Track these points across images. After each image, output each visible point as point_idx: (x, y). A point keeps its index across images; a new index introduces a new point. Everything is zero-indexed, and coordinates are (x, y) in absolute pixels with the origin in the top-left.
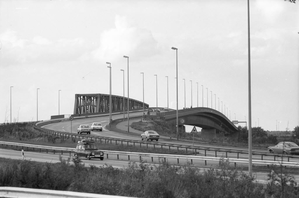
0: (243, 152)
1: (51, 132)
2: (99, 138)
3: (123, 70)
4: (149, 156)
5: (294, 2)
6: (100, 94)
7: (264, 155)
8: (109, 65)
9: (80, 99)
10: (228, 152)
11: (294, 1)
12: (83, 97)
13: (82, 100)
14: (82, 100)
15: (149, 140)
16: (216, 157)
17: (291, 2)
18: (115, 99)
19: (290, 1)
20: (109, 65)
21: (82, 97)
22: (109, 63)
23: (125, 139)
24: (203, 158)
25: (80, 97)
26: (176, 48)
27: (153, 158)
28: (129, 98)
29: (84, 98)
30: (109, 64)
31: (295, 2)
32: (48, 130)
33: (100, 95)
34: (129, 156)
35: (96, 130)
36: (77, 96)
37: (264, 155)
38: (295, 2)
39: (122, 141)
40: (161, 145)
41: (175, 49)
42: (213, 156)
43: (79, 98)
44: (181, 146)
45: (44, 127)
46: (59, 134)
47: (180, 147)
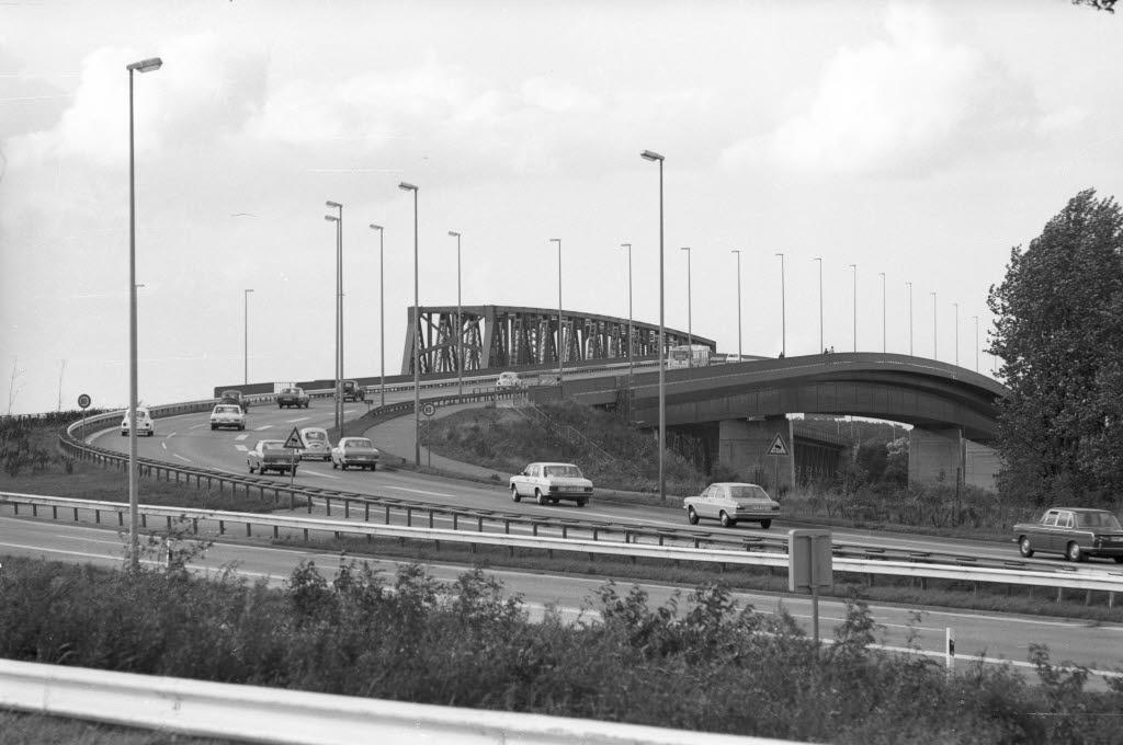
0: (885, 554)
1: (105, 457)
2: (288, 491)
3: (378, 228)
4: (161, 513)
5: (1109, 9)
6: (495, 307)
7: (437, 511)
8: (335, 212)
9: (430, 326)
10: (539, 524)
11: (1109, 4)
12: (442, 317)
13: (435, 332)
14: (435, 332)
15: (269, 471)
16: (455, 528)
17: (1099, 8)
18: (632, 330)
19: (1095, 4)
20: (335, 212)
21: (436, 318)
22: (335, 205)
23: (357, 492)
24: (359, 527)
25: (429, 320)
26: (415, 185)
27: (252, 527)
28: (666, 326)
29: (445, 321)
30: (413, 191)
31: (1113, 7)
32: (113, 453)
33: (495, 311)
34: (76, 509)
35: (355, 467)
36: (417, 314)
37: (602, 530)
38: (1113, 7)
39: (410, 509)
40: (504, 520)
41: (654, 157)
42: (499, 531)
43: (424, 324)
44: (549, 521)
45: (97, 440)
46: (183, 477)
47: (705, 540)
